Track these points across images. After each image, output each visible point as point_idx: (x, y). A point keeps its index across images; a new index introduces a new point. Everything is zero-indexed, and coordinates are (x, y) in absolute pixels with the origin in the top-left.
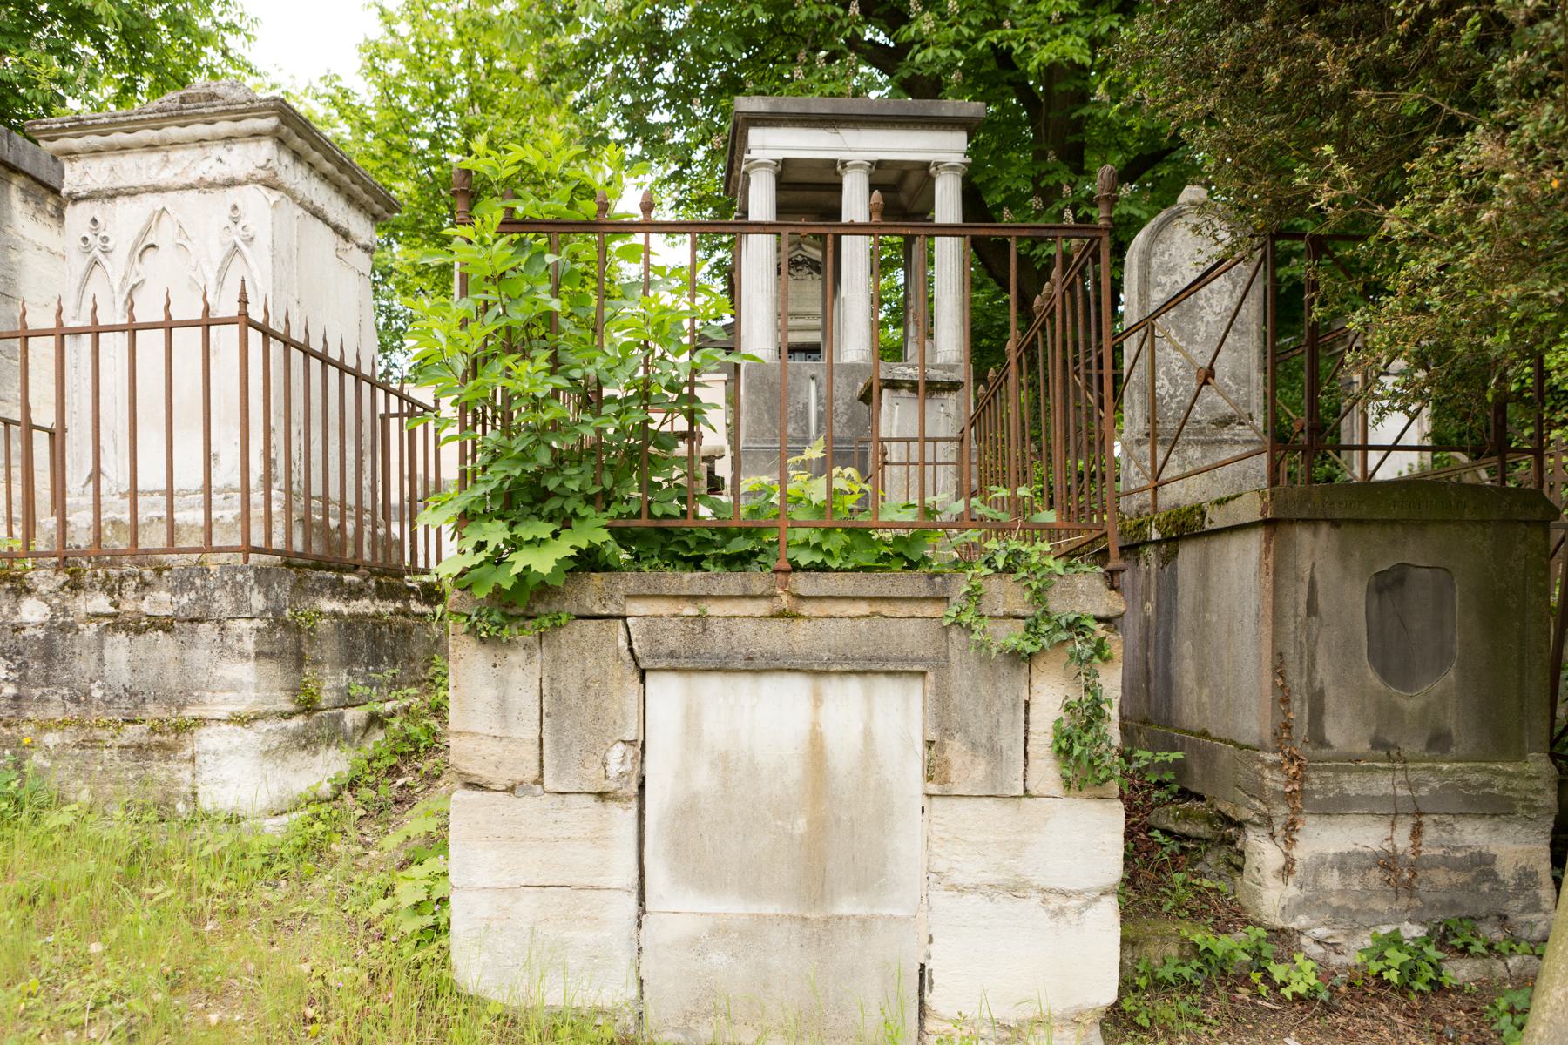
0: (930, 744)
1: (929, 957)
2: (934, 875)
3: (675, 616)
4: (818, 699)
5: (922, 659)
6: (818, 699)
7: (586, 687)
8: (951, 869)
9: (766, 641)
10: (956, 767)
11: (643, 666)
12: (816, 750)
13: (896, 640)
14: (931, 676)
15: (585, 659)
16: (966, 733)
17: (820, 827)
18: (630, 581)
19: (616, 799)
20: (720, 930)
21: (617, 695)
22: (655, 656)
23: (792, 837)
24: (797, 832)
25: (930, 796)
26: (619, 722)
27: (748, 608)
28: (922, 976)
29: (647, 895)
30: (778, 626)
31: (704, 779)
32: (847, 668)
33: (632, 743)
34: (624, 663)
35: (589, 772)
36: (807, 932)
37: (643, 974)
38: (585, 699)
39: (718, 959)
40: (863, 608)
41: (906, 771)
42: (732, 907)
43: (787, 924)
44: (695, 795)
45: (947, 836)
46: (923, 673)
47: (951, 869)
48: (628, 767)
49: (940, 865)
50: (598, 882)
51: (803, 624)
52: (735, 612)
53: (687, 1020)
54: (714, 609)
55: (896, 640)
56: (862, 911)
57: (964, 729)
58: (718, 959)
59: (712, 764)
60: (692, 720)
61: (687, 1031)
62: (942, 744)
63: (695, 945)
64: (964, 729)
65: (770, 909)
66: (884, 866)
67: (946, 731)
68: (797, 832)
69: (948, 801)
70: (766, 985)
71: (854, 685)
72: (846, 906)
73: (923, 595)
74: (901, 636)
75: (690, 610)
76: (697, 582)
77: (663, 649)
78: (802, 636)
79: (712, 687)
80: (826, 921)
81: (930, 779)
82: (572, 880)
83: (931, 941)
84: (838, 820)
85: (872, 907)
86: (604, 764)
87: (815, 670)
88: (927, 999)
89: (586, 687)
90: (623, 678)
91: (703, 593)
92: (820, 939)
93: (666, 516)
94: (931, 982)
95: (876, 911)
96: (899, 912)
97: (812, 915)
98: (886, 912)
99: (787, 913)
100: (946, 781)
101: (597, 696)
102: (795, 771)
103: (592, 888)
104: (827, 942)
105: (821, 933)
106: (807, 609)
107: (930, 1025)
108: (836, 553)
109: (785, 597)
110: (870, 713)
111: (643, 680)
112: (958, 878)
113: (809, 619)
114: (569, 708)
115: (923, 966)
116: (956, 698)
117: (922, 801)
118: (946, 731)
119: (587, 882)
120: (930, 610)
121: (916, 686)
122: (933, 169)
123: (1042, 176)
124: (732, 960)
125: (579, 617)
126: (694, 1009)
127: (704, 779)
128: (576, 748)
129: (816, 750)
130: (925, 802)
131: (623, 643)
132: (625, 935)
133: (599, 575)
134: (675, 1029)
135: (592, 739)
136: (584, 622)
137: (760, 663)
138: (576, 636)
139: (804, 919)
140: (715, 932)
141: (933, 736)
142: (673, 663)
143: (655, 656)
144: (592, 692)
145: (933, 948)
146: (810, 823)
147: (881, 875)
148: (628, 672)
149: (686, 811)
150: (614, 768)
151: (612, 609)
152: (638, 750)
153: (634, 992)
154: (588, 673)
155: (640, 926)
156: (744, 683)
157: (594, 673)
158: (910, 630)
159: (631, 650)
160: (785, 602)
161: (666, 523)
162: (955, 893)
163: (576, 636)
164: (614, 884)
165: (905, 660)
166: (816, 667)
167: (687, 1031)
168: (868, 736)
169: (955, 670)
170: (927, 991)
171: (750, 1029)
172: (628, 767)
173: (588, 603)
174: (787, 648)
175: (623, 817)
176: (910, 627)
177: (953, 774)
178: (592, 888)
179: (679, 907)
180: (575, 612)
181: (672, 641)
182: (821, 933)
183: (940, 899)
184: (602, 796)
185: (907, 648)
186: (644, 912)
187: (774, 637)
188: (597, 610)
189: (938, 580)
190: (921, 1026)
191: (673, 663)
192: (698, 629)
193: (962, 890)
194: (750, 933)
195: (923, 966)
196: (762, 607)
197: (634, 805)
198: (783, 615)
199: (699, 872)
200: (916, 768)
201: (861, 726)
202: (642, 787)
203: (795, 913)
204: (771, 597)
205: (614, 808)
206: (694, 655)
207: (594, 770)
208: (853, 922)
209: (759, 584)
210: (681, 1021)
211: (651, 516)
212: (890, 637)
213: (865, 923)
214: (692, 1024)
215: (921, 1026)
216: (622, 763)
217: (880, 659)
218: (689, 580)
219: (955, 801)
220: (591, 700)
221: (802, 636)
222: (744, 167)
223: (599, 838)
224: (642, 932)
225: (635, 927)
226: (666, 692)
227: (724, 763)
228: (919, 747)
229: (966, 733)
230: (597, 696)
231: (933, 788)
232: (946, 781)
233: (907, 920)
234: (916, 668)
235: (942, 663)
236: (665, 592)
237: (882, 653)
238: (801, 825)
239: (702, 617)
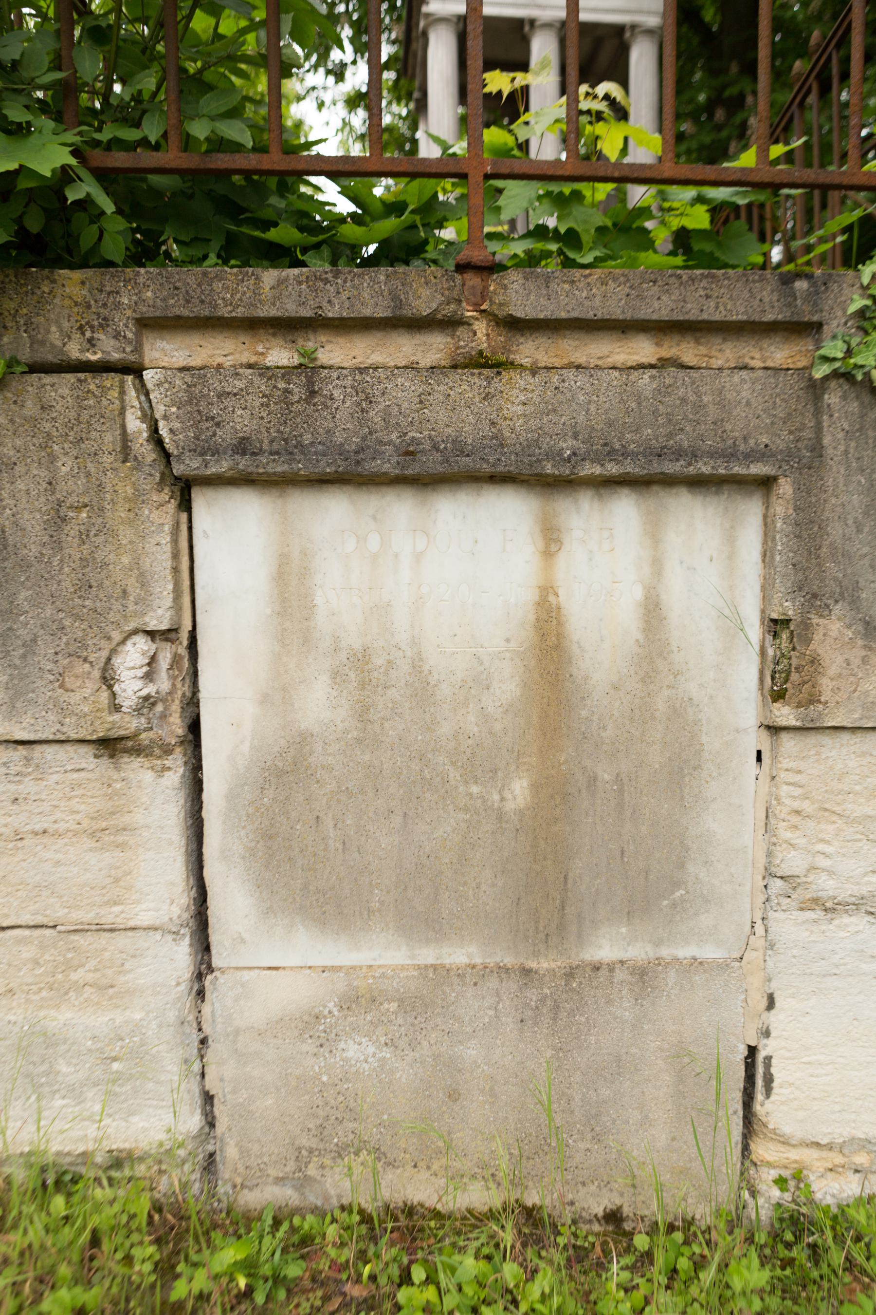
0: (776, 626)
1: (767, 1034)
2: (779, 882)
3: (250, 366)
4: (551, 539)
5: (763, 454)
6: (551, 539)
7: (58, 520)
8: (813, 868)
9: (442, 416)
10: (832, 671)
11: (178, 469)
12: (549, 640)
13: (713, 412)
14: (785, 487)
15: (53, 458)
16: (854, 603)
17: (557, 795)
18: (145, 289)
19: (138, 751)
20: (361, 999)
21: (126, 534)
22: (207, 449)
23: (500, 816)
24: (510, 806)
25: (774, 730)
26: (134, 592)
27: (404, 349)
28: (750, 1078)
29: (214, 938)
30: (468, 386)
31: (320, 705)
32: (613, 469)
33: (168, 635)
34: (139, 465)
35: (75, 698)
36: (533, 995)
37: (211, 1085)
38: (58, 546)
39: (358, 1051)
40: (643, 349)
41: (731, 684)
42: (384, 954)
43: (493, 982)
44: (304, 739)
45: (806, 806)
46: (766, 484)
47: (813, 868)
48: (163, 683)
49: (792, 862)
50: (110, 915)
51: (522, 380)
52: (377, 358)
53: (301, 1163)
54: (335, 352)
55: (713, 412)
56: (638, 952)
57: (849, 594)
58: (358, 1051)
59: (335, 674)
60: (291, 587)
61: (303, 1183)
62: (806, 625)
63: (311, 1025)
64: (849, 594)
65: (458, 955)
66: (681, 866)
67: (814, 599)
68: (510, 806)
69: (812, 739)
70: (454, 1096)
71: (625, 511)
72: (606, 947)
73: (769, 317)
74: (721, 404)
75: (280, 355)
76: (292, 288)
77: (224, 436)
78: (517, 405)
79: (332, 517)
80: (570, 974)
81: (778, 696)
82: (58, 913)
83: (771, 1003)
84: (593, 780)
85: (658, 943)
86: (108, 680)
87: (544, 475)
88: (757, 1108)
89: (58, 520)
90: (137, 499)
91: (306, 312)
92: (556, 1008)
93: (219, 144)
94: (769, 1080)
95: (665, 952)
96: (710, 952)
97: (543, 964)
98: (684, 952)
99: (491, 961)
100: (813, 700)
101: (83, 537)
102: (507, 687)
103: (101, 929)
104: (571, 1013)
105: (559, 996)
106: (529, 350)
107: (761, 1150)
108: (587, 238)
109: (481, 327)
110: (657, 565)
111: (186, 505)
112: (826, 886)
113: (534, 371)
114: (25, 565)
115: (752, 1051)
116: (836, 531)
117: (755, 739)
118: (814, 599)
119: (87, 916)
120: (781, 353)
121: (750, 512)
122: (627, 35)
123: (724, 87)
124: (387, 1053)
125: (36, 368)
126: (314, 1143)
127: (320, 705)
128: (45, 649)
129: (549, 640)
130: (764, 741)
131: (135, 424)
132: (172, 1015)
133: (77, 275)
134: (279, 1181)
135: (77, 629)
136: (47, 379)
137: (432, 463)
138: (31, 408)
139: (526, 972)
140: (351, 1002)
141: (789, 609)
142: (244, 463)
143: (207, 449)
144: (72, 530)
145: (775, 1019)
146: (535, 788)
147: (676, 885)
148: (147, 485)
149: (285, 770)
150: (130, 687)
151: (108, 349)
152: (183, 651)
153: (194, 1121)
154: (62, 488)
155: (201, 994)
156: (399, 509)
157: (73, 488)
158: (741, 388)
159: (157, 441)
160: (481, 335)
161: (222, 161)
162: (819, 914)
163: (31, 408)
164: (145, 918)
165: (731, 455)
166: (549, 468)
167: (303, 1183)
168: (652, 612)
169: (835, 473)
170: (759, 1096)
171: (424, 1175)
172: (163, 683)
173: (55, 337)
174: (487, 430)
175: (155, 790)
176: (743, 390)
177: (826, 684)
178: (101, 929)
179: (277, 962)
180: (25, 355)
181: (242, 420)
182: (559, 996)
183: (790, 925)
184: (110, 746)
185: (735, 429)
186: (210, 969)
187: (459, 410)
188: (75, 351)
189: (801, 285)
190: (746, 1149)
191: (244, 463)
192: (298, 392)
193: (830, 908)
194: (424, 1000)
195: (752, 1051)
196: (432, 349)
197: (177, 763)
198: (480, 362)
199: (314, 893)
200: (746, 675)
201: (638, 593)
202: (194, 727)
203: (509, 960)
204: (450, 324)
205: (137, 772)
206: (290, 447)
207: (85, 693)
208: (620, 975)
209: (425, 292)
210: (291, 1166)
211: (188, 142)
212: (699, 407)
213: (644, 975)
214: (312, 1171)
215: (746, 1149)
216: (149, 677)
217: (679, 454)
218: (272, 288)
219: (826, 739)
220: (73, 549)
221: (517, 405)
222: (422, 24)
223: (108, 830)
224: (206, 1008)
225: (189, 1002)
226: (235, 534)
227: (360, 672)
228: (755, 631)
229: (854, 603)
230: (83, 537)
231: (785, 714)
232: (813, 700)
233: (723, 966)
234: (758, 469)
235: (809, 459)
236: (224, 311)
237: (684, 440)
238: (519, 791)
239: (309, 370)
